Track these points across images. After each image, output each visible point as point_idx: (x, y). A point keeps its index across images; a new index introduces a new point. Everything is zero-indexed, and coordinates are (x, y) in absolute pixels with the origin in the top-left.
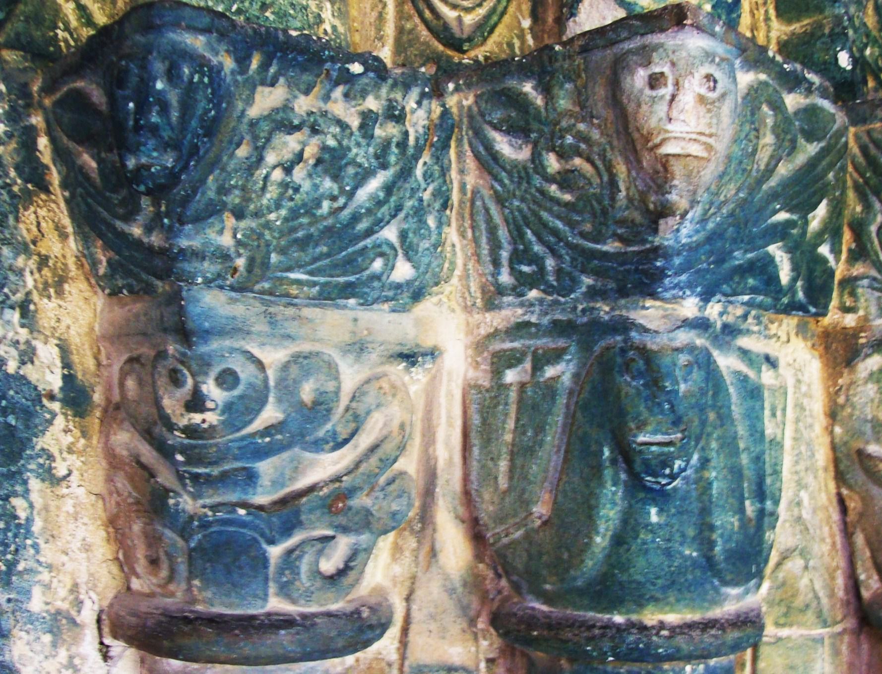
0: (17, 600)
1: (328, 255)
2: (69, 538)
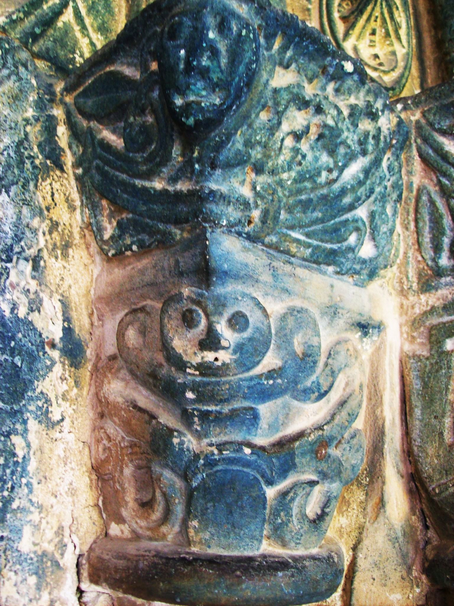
0: (9, 539)
1: (322, 221)
2: (59, 481)
